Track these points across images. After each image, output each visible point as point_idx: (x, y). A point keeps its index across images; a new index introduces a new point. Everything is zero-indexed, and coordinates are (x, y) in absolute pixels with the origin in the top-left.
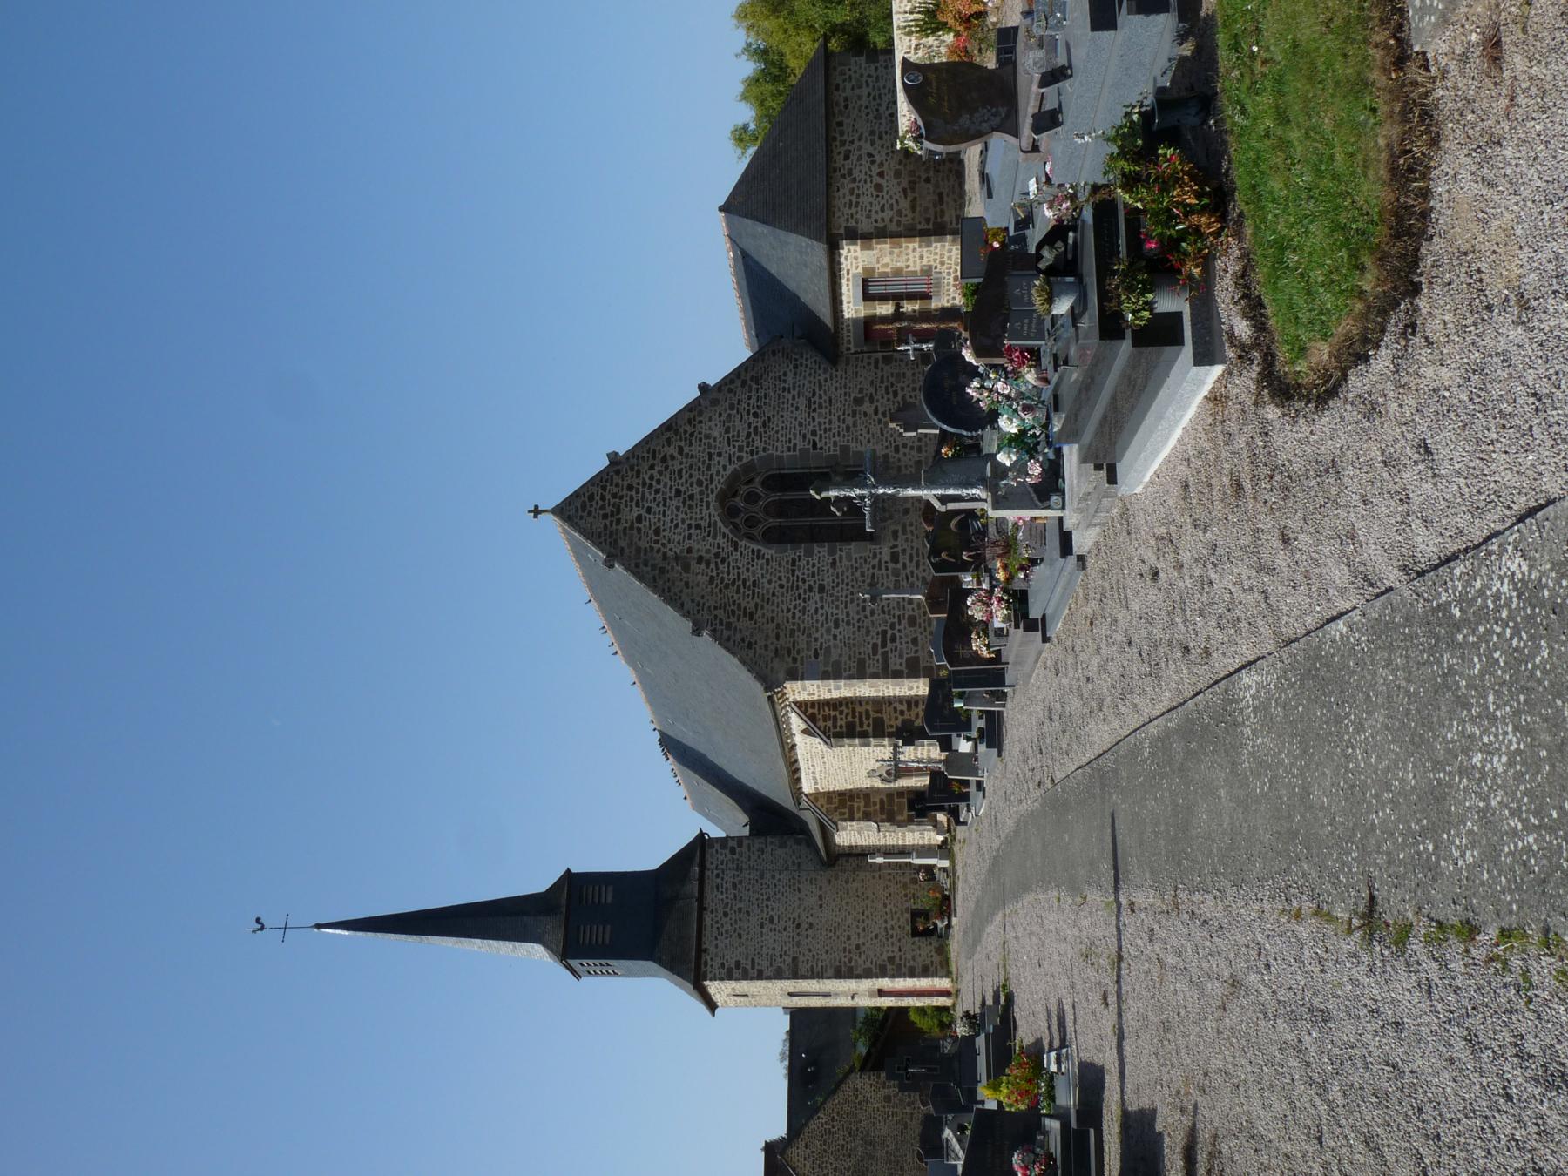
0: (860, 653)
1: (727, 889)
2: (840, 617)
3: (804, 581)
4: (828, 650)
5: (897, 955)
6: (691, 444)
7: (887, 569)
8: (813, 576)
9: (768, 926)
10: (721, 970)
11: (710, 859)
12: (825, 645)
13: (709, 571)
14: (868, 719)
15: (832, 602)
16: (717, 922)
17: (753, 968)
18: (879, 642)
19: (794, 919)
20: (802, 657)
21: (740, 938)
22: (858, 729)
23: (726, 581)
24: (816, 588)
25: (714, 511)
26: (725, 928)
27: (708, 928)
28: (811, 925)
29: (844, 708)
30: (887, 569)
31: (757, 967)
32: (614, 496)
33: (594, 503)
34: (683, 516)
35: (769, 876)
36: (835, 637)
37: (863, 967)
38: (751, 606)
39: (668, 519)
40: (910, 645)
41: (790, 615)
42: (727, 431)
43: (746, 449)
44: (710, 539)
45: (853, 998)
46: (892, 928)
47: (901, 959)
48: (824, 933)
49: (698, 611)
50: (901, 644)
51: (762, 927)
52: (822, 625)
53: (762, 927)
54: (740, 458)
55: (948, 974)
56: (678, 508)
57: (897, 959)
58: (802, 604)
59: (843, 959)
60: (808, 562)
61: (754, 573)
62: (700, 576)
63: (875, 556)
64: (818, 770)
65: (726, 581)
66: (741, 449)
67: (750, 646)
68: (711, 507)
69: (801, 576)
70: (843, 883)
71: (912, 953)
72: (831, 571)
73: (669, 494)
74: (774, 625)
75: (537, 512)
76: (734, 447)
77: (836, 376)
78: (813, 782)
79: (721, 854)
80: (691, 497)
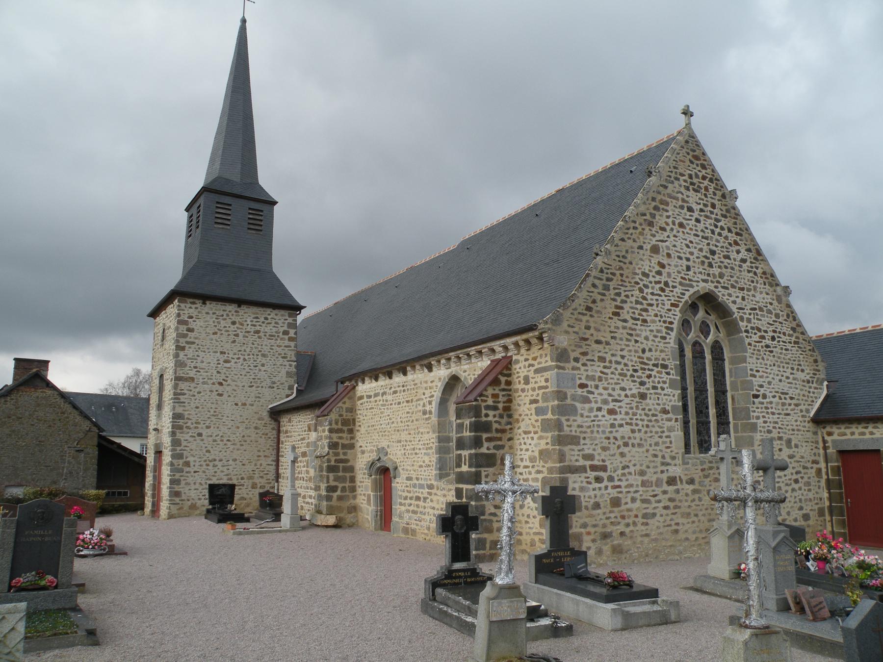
0: (584, 438)
1: (255, 326)
2: (618, 417)
3: (649, 376)
4: (586, 400)
5: (191, 469)
6: (749, 272)
7: (662, 472)
8: (655, 388)
9: (222, 358)
10: (187, 315)
11: (280, 314)
12: (591, 396)
13: (654, 274)
14: (495, 447)
15: (632, 408)
16: (228, 315)
17: (187, 343)
18: (596, 462)
19: (227, 381)
20: (579, 369)
21: (213, 334)
22: (485, 436)
23: (646, 290)
24: (643, 390)
25: (702, 287)
26: (222, 322)
27: (223, 307)
28: (221, 395)
29: (505, 419)
30: (662, 472)
31: (187, 346)
32: (706, 189)
33: (699, 168)
34: (696, 255)
35: (264, 361)
36: (599, 409)
37: (182, 439)
38: (625, 315)
39: (692, 238)
40: (592, 501)
41: (619, 359)
42: (761, 309)
43: (749, 325)
44: (679, 279)
45: (155, 430)
46: (214, 466)
47: (187, 472)
48: (213, 406)
49: (618, 256)
50: (594, 489)
51: (222, 353)
52: (610, 395)
53: (222, 353)
54: (742, 319)
55: (171, 516)
56: (701, 250)
57: (188, 469)
58: (629, 374)
59: (190, 422)
60: (665, 382)
61: (653, 322)
62: (649, 263)
63: (673, 458)
64: (390, 398)
65: (646, 290)
66: (749, 321)
67: (589, 309)
68: (704, 284)
69: (653, 373)
70: (255, 425)
71: (192, 483)
72: (659, 408)
73: (711, 243)
74: (609, 339)
75: (687, 113)
76: (750, 314)
77: (805, 421)
78: (372, 394)
79: (284, 323)
80: (710, 265)
